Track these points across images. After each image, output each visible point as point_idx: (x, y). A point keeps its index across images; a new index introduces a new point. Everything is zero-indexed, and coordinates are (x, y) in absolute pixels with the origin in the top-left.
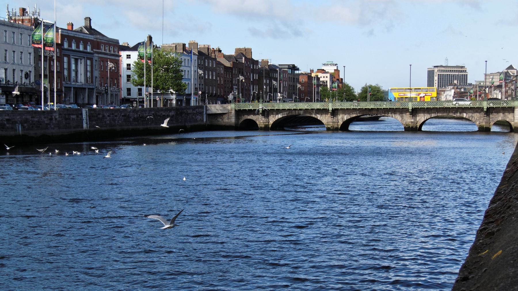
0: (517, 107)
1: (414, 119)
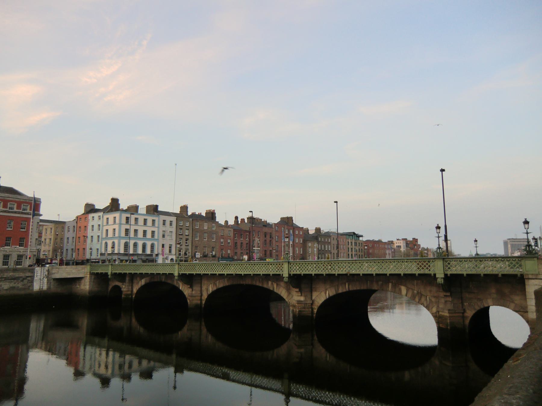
0: (530, 277)
1: (305, 296)
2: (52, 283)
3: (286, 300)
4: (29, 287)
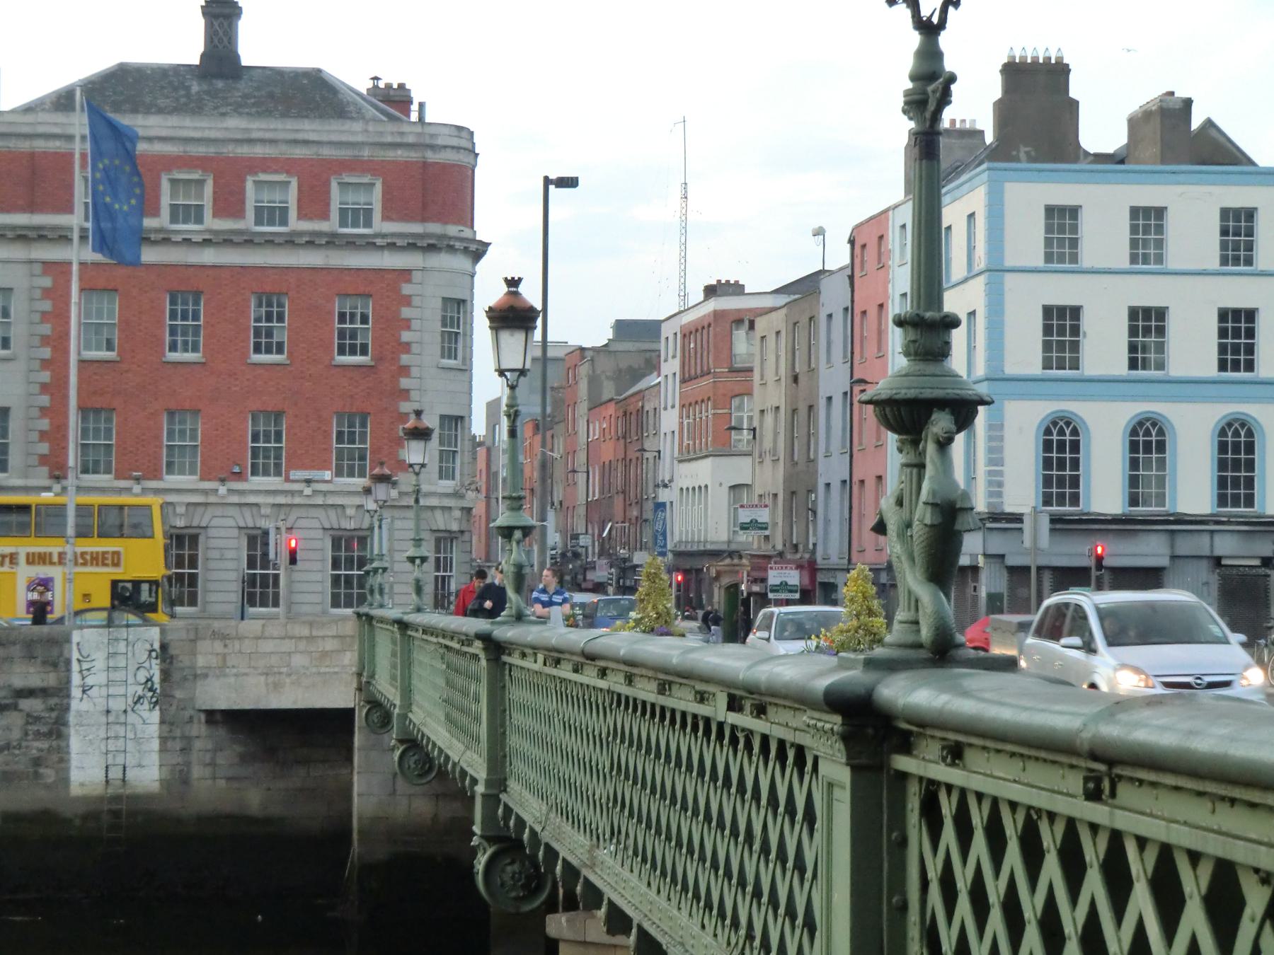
2: (198, 745)
4: (37, 762)
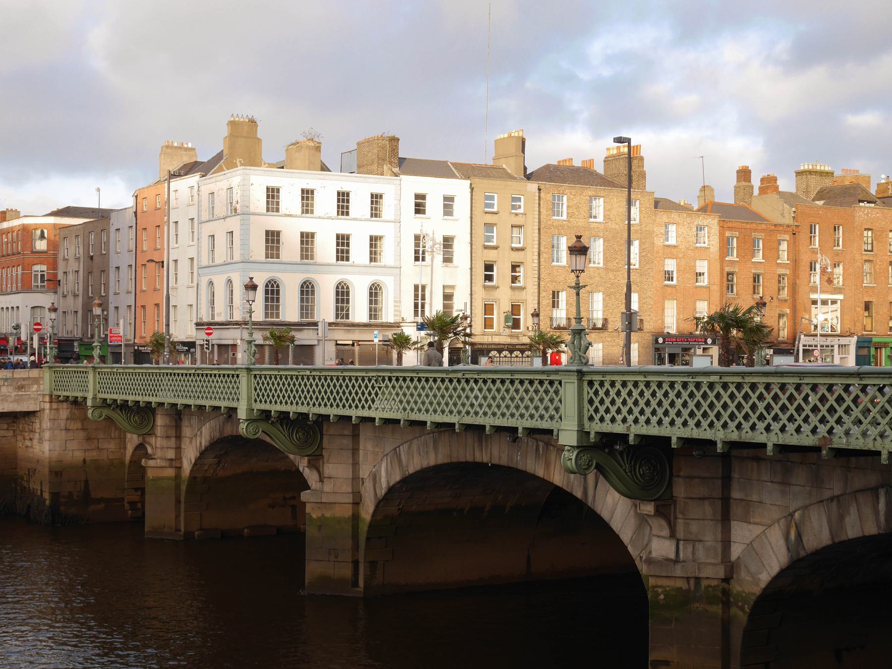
3: (630, 548)
